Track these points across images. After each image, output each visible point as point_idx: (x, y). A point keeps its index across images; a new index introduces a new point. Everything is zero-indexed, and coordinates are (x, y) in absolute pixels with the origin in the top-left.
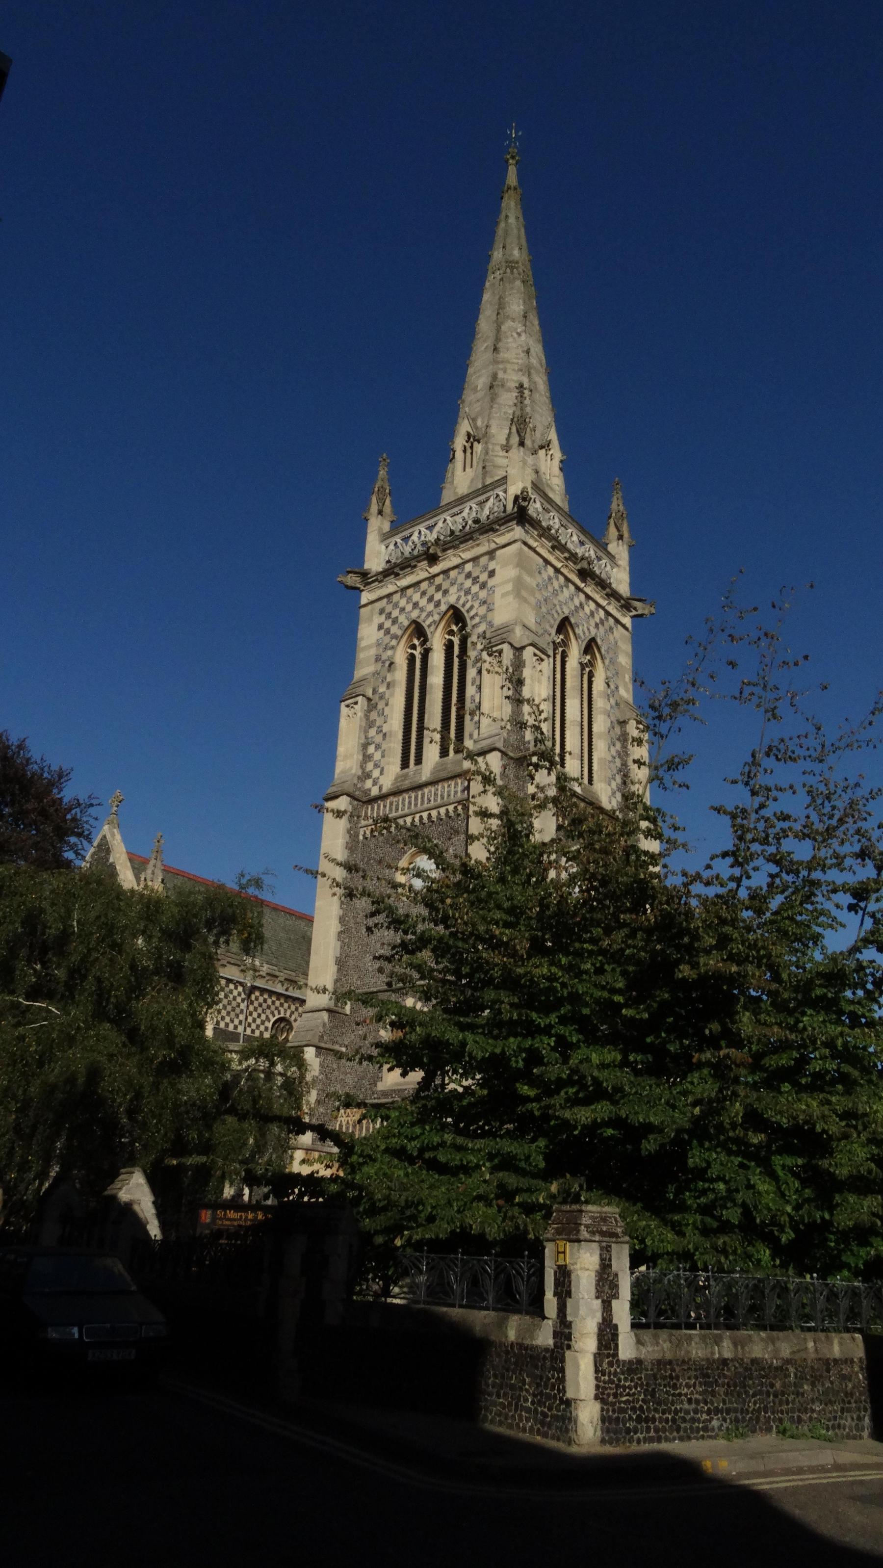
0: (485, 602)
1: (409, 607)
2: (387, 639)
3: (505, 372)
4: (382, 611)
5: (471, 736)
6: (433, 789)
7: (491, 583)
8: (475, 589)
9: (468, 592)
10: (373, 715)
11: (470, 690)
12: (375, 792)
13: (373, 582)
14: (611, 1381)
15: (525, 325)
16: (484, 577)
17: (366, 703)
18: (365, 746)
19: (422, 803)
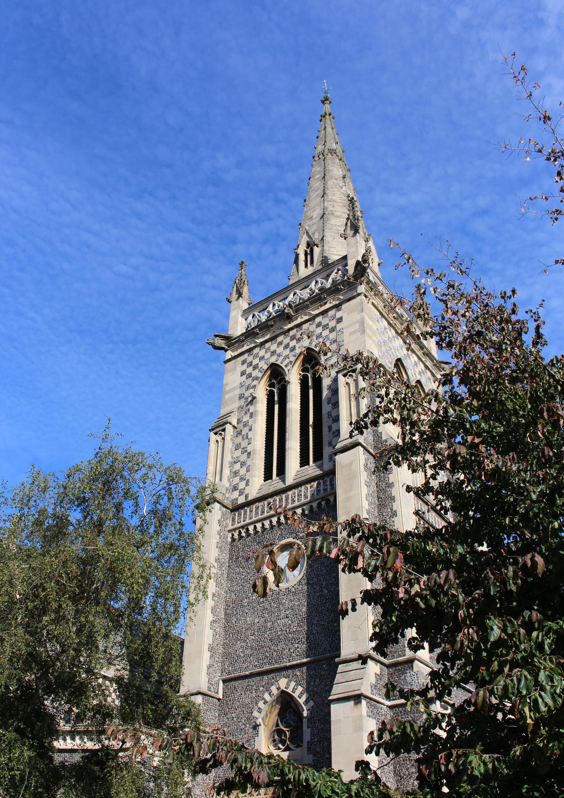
0: (335, 341)
1: (267, 356)
2: (249, 381)
3: (333, 207)
4: (244, 362)
7: (339, 327)
12: (242, 500)
13: (236, 342)
15: (344, 182)
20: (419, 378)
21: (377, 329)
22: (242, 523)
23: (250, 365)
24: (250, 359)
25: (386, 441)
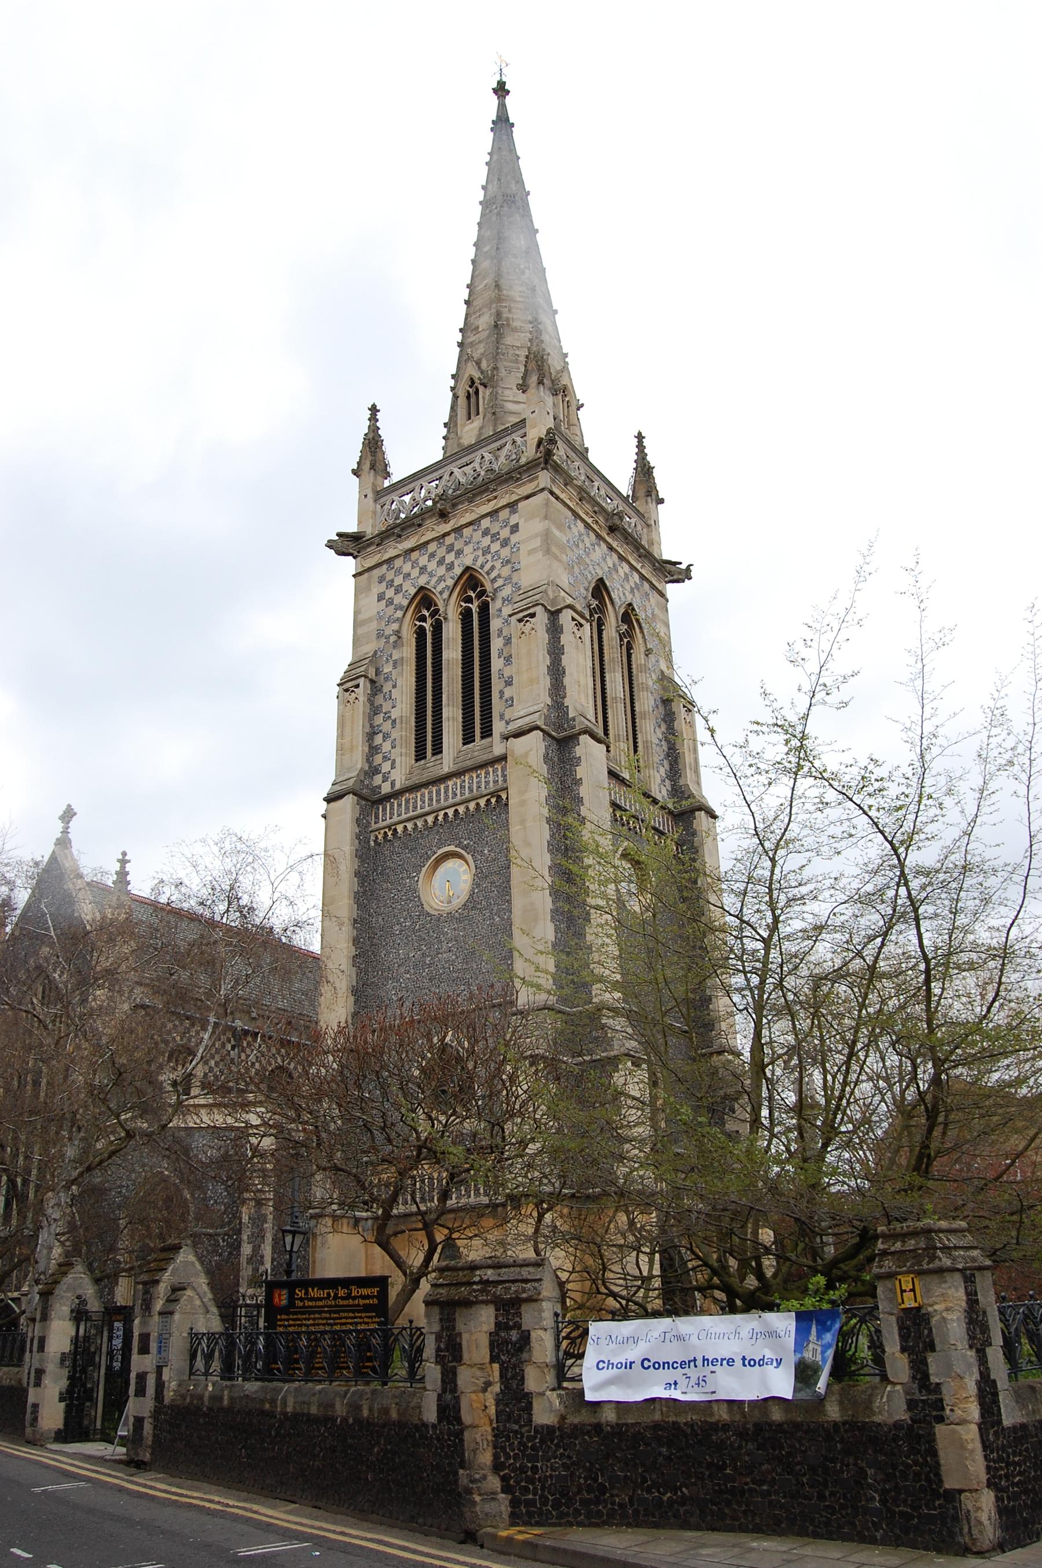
0: (508, 562)
1: (415, 573)
4: (382, 579)
5: (502, 716)
6: (426, 792)
7: (514, 539)
8: (495, 547)
9: (486, 551)
10: (379, 700)
11: (496, 664)
12: (386, 789)
14: (1000, 1459)
16: (505, 533)
17: (368, 685)
18: (371, 736)
19: (446, 799)
20: (629, 598)
21: (568, 541)
22: (388, 822)
23: (392, 586)
24: (390, 575)
25: (574, 719)
